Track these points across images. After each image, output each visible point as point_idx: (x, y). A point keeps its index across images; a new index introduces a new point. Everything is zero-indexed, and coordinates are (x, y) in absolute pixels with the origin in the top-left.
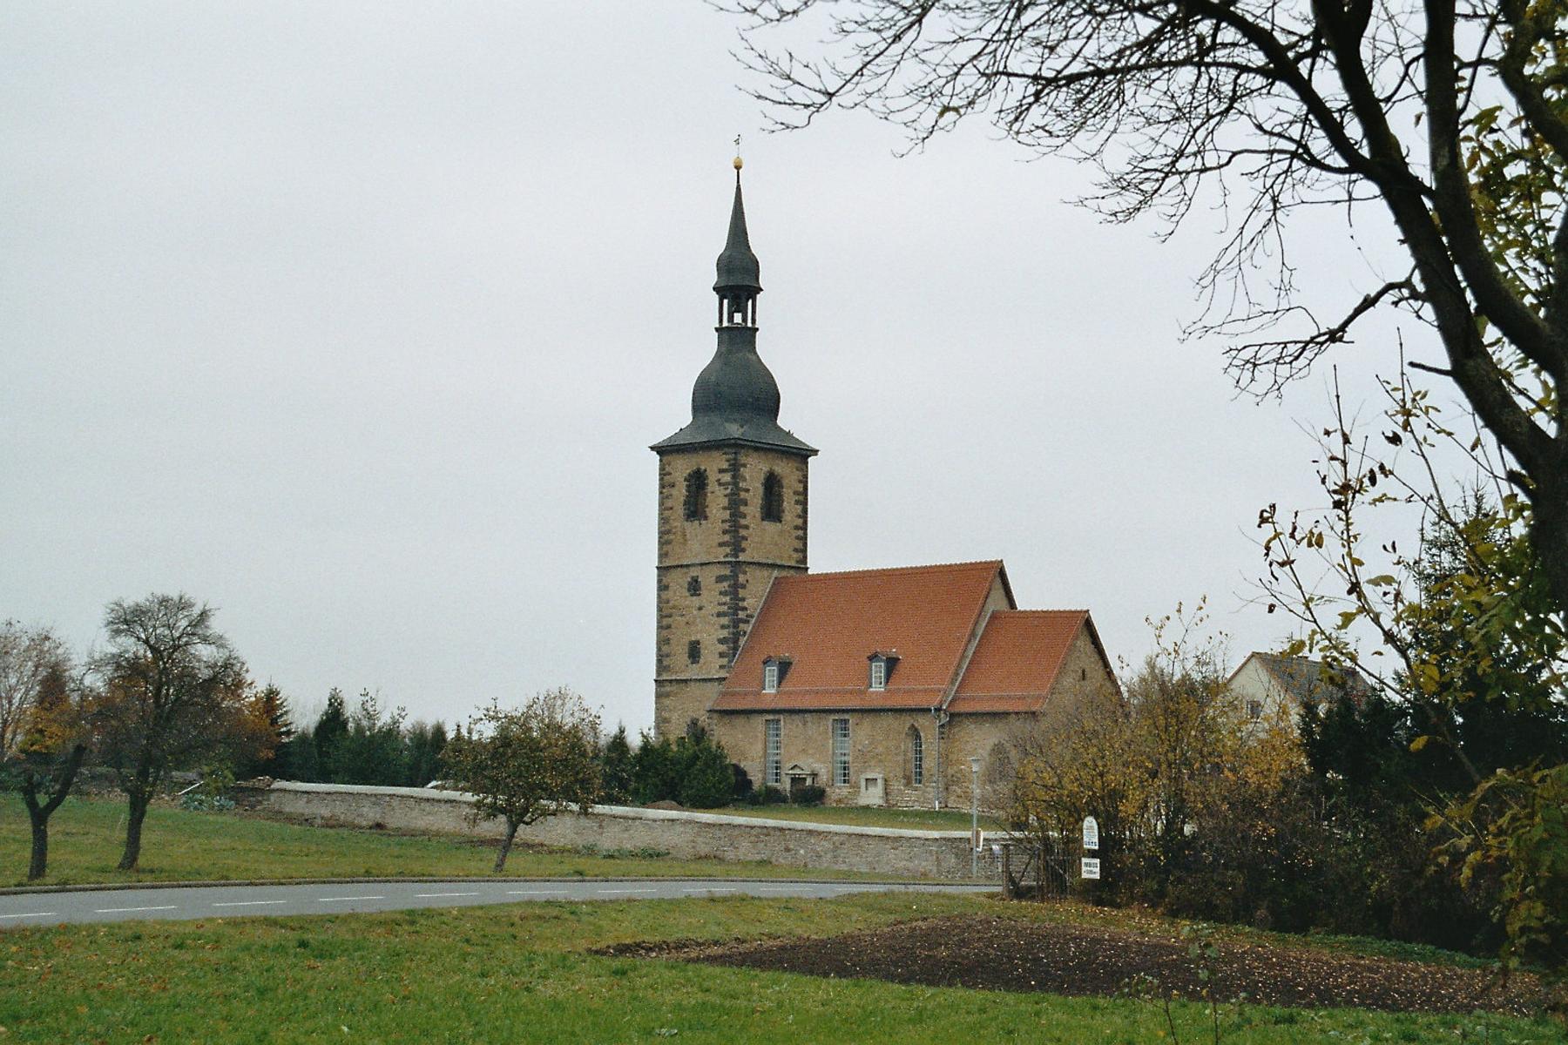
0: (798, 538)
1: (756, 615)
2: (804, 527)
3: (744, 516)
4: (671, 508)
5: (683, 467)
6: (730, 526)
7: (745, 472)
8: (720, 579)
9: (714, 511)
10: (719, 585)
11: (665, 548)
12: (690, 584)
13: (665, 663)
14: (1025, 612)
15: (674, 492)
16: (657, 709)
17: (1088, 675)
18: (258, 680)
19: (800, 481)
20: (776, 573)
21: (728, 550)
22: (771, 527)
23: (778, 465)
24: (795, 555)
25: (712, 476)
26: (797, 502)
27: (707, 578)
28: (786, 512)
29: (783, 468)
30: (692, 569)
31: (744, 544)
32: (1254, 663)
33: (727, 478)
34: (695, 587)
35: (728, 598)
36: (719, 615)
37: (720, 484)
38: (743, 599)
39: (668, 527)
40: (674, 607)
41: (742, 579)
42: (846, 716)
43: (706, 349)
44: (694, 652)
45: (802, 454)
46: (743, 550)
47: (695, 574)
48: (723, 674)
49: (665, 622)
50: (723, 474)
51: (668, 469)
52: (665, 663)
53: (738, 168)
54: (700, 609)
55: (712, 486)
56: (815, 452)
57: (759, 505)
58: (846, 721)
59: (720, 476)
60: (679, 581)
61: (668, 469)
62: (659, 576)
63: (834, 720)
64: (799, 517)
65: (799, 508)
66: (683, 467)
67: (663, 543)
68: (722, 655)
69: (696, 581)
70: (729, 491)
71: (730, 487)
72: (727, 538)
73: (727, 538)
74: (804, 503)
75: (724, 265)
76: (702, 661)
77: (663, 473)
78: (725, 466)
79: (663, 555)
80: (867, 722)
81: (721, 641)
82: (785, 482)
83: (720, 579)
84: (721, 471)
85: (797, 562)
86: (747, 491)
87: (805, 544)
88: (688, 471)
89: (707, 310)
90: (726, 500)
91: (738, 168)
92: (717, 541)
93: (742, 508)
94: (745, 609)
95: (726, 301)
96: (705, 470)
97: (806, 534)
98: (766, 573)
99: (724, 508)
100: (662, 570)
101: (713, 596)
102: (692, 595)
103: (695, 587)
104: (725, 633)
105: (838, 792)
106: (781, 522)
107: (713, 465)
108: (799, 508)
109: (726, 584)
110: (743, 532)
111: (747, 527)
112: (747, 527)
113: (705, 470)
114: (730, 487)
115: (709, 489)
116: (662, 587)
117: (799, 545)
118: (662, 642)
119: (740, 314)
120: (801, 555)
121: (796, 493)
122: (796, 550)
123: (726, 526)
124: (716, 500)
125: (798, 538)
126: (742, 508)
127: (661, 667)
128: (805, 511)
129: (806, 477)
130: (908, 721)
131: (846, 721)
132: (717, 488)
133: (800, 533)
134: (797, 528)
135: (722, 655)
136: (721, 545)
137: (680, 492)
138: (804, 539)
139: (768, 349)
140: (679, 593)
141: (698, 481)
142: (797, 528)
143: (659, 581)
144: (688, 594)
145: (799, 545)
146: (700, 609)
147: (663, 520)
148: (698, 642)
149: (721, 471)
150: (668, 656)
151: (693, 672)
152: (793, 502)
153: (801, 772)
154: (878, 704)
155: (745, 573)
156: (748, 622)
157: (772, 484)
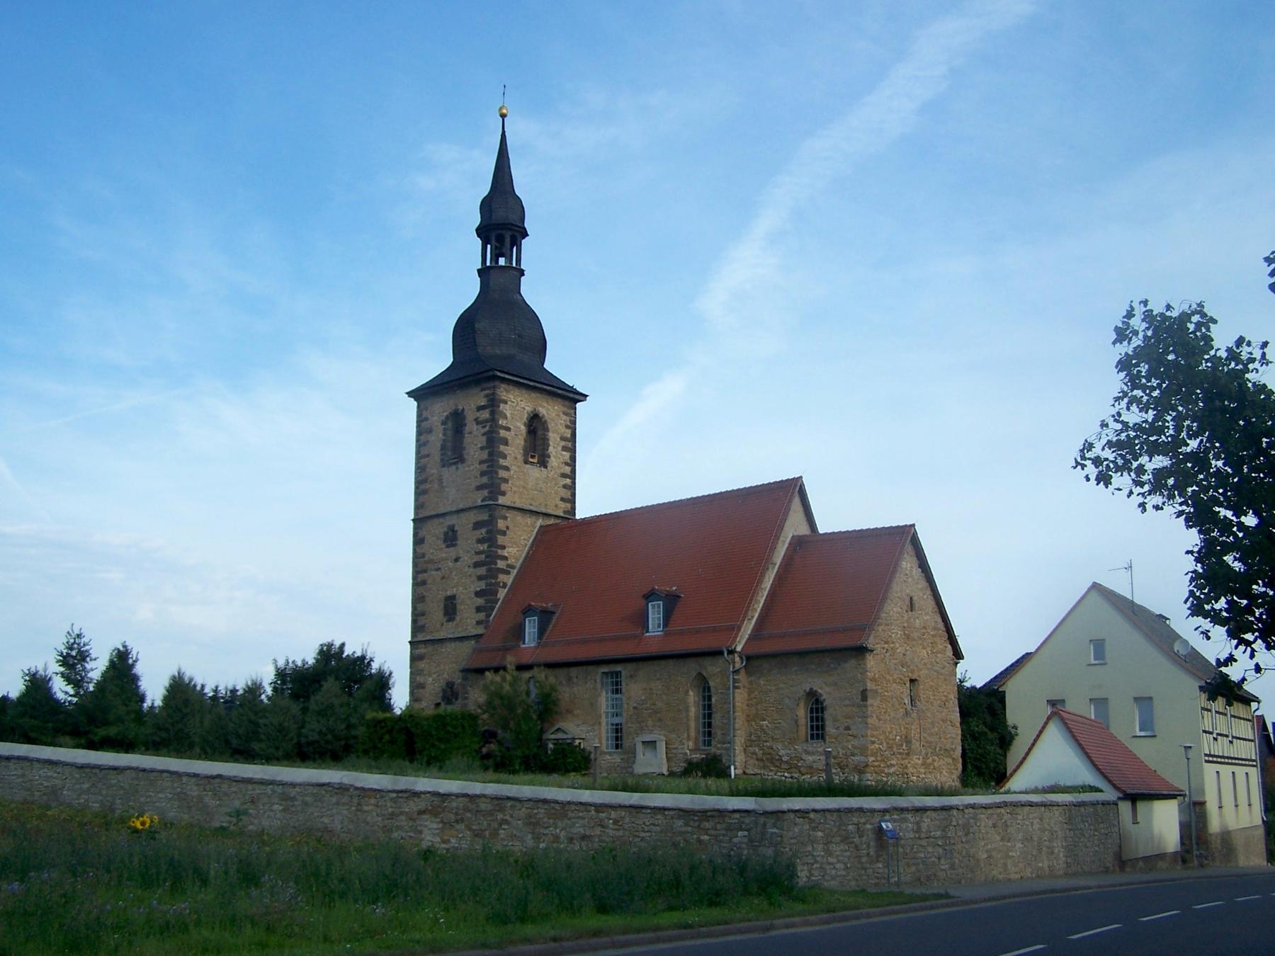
0: (565, 486)
1: (518, 566)
2: (572, 475)
3: (505, 457)
4: (428, 455)
5: (441, 408)
6: (488, 467)
7: (506, 409)
8: (477, 525)
9: (472, 453)
10: (475, 532)
11: (422, 499)
12: (446, 534)
13: (420, 623)
14: (826, 534)
15: (432, 438)
16: (411, 673)
17: (917, 606)
18: (392, 701)
19: (567, 427)
20: (540, 522)
21: (486, 493)
22: (535, 472)
23: (541, 406)
24: (562, 505)
25: (470, 416)
26: (564, 449)
27: (464, 524)
28: (552, 458)
29: (550, 410)
30: (448, 518)
31: (504, 487)
32: (1094, 594)
33: (485, 415)
34: (451, 538)
35: (486, 546)
36: (476, 565)
37: (478, 423)
38: (504, 547)
39: (424, 477)
40: (431, 561)
41: (501, 524)
42: (618, 668)
43: (470, 290)
44: (450, 606)
45: (571, 397)
46: (503, 494)
47: (450, 523)
48: (480, 630)
49: (420, 577)
50: (481, 412)
51: (425, 414)
52: (420, 623)
53: (503, 116)
54: (457, 560)
55: (471, 427)
56: (584, 397)
57: (521, 447)
58: (618, 674)
59: (478, 414)
60: (436, 530)
61: (425, 414)
62: (415, 528)
63: (603, 673)
64: (567, 464)
65: (567, 455)
66: (441, 408)
67: (420, 491)
68: (479, 609)
69: (453, 531)
70: (487, 428)
71: (489, 424)
72: (485, 480)
73: (485, 480)
74: (573, 451)
75: (487, 206)
76: (458, 618)
77: (421, 420)
78: (483, 402)
79: (418, 507)
80: (644, 670)
81: (478, 594)
82: (551, 425)
83: (477, 525)
84: (480, 408)
85: (564, 512)
86: (508, 429)
87: (574, 495)
88: (445, 414)
89: (471, 251)
90: (484, 438)
91: (503, 116)
92: (474, 485)
93: (502, 448)
94: (506, 558)
95: (489, 246)
96: (463, 410)
97: (574, 483)
98: (529, 520)
99: (482, 448)
100: (418, 522)
101: (469, 545)
102: (448, 547)
103: (451, 538)
104: (482, 585)
105: (608, 759)
106: (546, 467)
107: (471, 402)
108: (567, 455)
109: (484, 531)
110: (502, 474)
111: (507, 469)
112: (507, 469)
113: (463, 410)
114: (489, 424)
115: (467, 429)
116: (418, 541)
117: (567, 494)
118: (418, 599)
119: (504, 259)
120: (569, 505)
121: (563, 439)
122: (563, 499)
123: (484, 467)
124: (474, 439)
125: (565, 486)
126: (502, 448)
127: (417, 627)
128: (573, 459)
129: (574, 422)
130: (692, 666)
131: (618, 674)
132: (475, 427)
133: (568, 481)
134: (564, 476)
135: (479, 609)
136: (479, 488)
137: (437, 438)
138: (572, 488)
139: (532, 291)
140: (435, 548)
141: (457, 420)
142: (564, 476)
143: (415, 535)
144: (443, 546)
145: (567, 494)
146: (457, 560)
147: (420, 469)
148: (453, 597)
149: (480, 408)
150: (423, 614)
151: (448, 631)
152: (560, 448)
153: (565, 737)
154: (654, 649)
155: (505, 518)
156: (508, 573)
157: (536, 425)
